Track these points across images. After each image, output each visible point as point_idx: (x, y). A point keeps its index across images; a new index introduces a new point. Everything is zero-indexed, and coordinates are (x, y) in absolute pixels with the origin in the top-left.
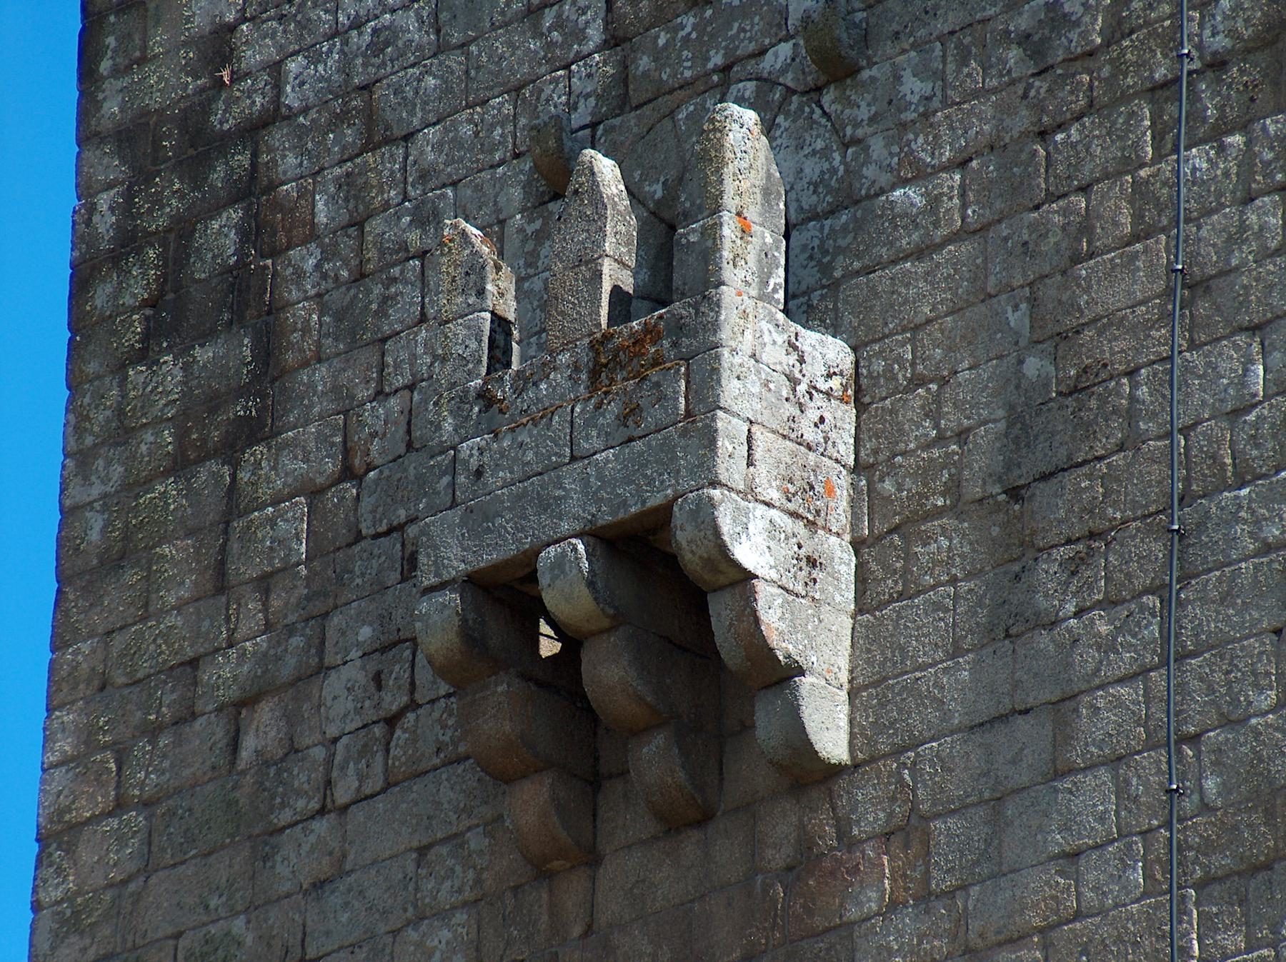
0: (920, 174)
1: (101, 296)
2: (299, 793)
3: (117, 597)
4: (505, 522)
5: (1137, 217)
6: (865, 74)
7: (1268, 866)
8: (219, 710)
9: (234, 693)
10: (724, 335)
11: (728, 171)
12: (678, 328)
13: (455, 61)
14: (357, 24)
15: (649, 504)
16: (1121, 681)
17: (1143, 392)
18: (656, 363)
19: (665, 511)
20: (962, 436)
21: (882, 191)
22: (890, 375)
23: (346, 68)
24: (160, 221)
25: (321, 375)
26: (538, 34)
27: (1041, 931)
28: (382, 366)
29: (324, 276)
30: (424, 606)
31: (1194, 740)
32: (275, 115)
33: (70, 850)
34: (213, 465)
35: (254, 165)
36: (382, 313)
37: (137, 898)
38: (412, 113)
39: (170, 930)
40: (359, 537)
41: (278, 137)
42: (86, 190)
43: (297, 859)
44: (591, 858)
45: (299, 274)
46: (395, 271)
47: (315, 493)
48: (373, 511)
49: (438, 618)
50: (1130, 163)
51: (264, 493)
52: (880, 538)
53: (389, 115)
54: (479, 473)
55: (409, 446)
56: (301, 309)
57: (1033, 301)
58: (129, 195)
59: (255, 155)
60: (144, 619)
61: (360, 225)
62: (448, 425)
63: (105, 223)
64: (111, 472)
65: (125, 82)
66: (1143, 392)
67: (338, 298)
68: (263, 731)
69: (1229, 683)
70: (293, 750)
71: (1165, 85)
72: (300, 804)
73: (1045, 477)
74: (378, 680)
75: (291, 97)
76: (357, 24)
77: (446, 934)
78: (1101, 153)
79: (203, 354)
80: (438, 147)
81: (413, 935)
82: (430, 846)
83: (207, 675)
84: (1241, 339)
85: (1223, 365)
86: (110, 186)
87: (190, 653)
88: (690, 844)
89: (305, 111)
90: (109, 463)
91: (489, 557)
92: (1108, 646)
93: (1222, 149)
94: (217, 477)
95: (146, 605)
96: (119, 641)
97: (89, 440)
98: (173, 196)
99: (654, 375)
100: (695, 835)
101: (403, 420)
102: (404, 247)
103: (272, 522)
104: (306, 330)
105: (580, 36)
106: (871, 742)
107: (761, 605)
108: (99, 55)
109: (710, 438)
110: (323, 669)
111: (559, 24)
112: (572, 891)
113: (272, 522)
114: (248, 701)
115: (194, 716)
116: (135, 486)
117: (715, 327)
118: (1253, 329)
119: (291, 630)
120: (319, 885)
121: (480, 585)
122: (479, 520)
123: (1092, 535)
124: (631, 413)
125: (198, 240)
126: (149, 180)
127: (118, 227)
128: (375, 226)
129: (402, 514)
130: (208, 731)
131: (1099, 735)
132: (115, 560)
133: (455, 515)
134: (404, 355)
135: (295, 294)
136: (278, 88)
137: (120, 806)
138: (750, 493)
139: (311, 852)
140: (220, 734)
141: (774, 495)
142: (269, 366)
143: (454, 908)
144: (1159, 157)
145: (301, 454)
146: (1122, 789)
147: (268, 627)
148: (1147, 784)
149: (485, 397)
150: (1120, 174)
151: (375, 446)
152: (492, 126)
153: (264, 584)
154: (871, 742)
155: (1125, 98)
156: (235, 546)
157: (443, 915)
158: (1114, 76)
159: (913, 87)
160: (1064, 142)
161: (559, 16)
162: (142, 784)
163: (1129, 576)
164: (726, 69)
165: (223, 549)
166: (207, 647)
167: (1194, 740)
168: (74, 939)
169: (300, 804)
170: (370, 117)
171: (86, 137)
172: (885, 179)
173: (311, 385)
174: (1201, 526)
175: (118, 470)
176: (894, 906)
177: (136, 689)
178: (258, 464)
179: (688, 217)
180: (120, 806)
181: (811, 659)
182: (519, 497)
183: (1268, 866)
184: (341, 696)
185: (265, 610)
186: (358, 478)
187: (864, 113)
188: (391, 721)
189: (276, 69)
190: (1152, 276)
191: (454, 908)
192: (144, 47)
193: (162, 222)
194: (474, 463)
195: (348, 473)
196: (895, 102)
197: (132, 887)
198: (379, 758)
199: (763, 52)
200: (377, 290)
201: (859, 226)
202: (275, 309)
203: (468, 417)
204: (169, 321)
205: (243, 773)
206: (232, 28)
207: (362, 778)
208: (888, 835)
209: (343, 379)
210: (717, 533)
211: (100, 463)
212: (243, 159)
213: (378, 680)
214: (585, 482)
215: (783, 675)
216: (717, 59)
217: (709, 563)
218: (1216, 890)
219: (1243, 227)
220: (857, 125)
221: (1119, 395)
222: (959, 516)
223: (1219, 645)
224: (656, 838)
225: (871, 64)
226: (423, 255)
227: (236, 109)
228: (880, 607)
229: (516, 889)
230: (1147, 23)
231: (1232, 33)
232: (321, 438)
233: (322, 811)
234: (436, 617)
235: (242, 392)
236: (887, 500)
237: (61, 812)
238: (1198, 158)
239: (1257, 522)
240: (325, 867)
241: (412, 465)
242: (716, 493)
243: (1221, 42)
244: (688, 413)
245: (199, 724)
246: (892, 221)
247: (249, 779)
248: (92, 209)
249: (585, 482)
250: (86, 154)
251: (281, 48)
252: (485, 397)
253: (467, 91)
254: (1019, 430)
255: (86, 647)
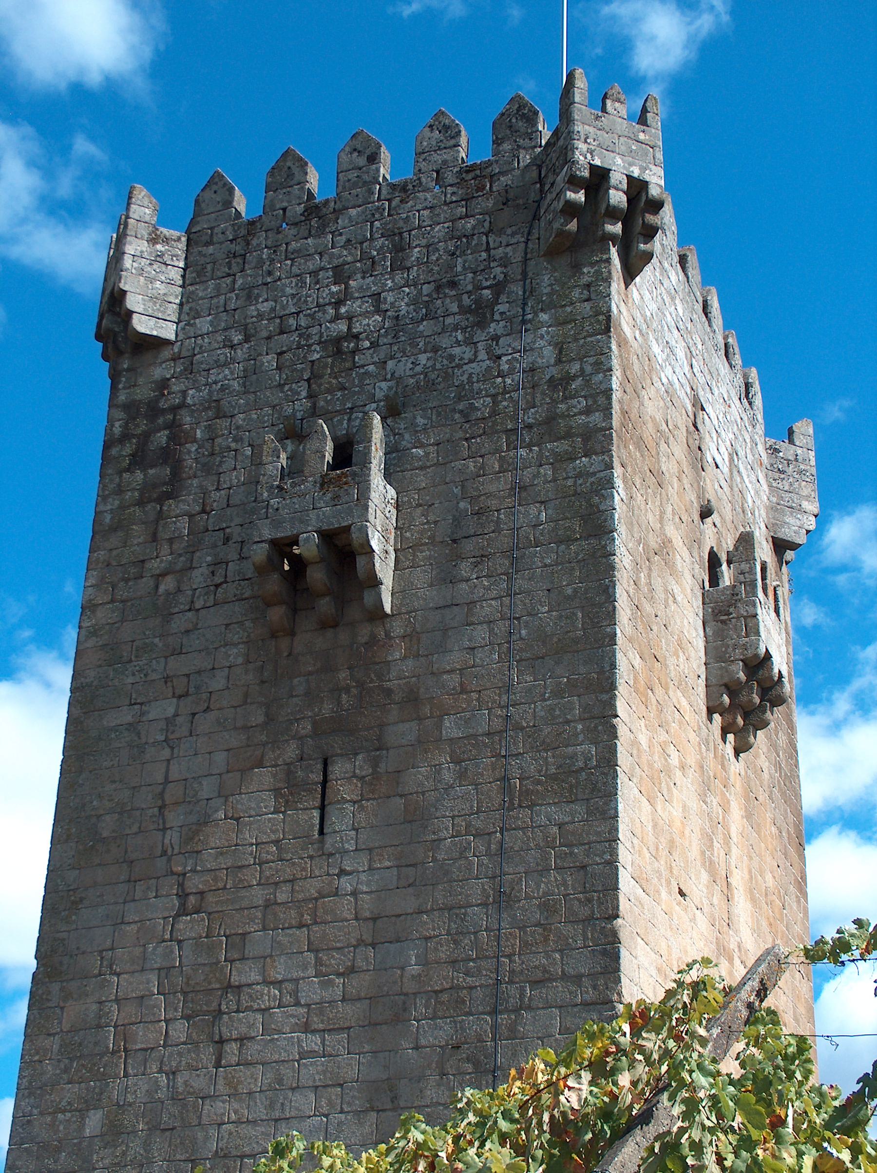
0: (422, 446)
1: (114, 451)
2: (181, 604)
3: (114, 540)
4: (287, 525)
5: (501, 466)
6: (403, 415)
7: (543, 658)
8: (152, 576)
9: (158, 572)
10: (371, 478)
11: (373, 431)
12: (354, 474)
13: (252, 397)
14: (215, 383)
15: (343, 525)
16: (492, 599)
17: (502, 516)
18: (346, 483)
19: (349, 527)
20: (436, 522)
21: (408, 449)
22: (409, 502)
23: (210, 393)
24: (139, 431)
25: (195, 482)
26: (282, 392)
27: (460, 670)
28: (219, 481)
29: (199, 453)
30: (255, 547)
31: (518, 619)
32: (183, 405)
33: (93, 612)
34: (153, 504)
35: (174, 418)
36: (220, 465)
37: (118, 628)
38: (234, 409)
39: (130, 639)
40: (207, 530)
41: (183, 412)
42: (110, 421)
43: (179, 623)
44: (293, 634)
45: (189, 452)
46: (226, 454)
47: (191, 516)
48: (214, 523)
49: (260, 552)
50: (499, 451)
51: (173, 514)
52: (404, 549)
53: (225, 409)
54: (277, 509)
55: (228, 506)
56: (189, 462)
57: (463, 487)
58: (127, 424)
59: (175, 416)
60: (124, 547)
61: (213, 440)
62: (266, 494)
63: (117, 429)
64: (114, 503)
65: (128, 391)
66: (502, 516)
67: (203, 460)
68: (168, 584)
69: (531, 604)
70: (179, 590)
71: (511, 430)
72: (182, 607)
73: (466, 537)
74: (213, 573)
75: (189, 401)
76: (215, 383)
77: (235, 651)
78: (487, 446)
79: (151, 472)
80: (244, 420)
81: (223, 650)
82: (230, 624)
83: (148, 565)
84: (537, 505)
85: (531, 512)
86: (120, 420)
87: (142, 558)
88: (330, 633)
89: (194, 405)
90: (114, 500)
91: (279, 535)
92: (488, 589)
93: (531, 450)
94: (155, 508)
95: (126, 543)
96: (115, 553)
97: (107, 492)
98: (142, 425)
99: (346, 487)
100: (332, 630)
101: (226, 498)
102: (230, 447)
103: (175, 523)
104: (191, 468)
105: (299, 394)
106: (399, 609)
107: (375, 561)
108: (119, 382)
109: (366, 508)
110: (191, 568)
111: (290, 389)
112: (284, 643)
113: (175, 523)
114: (163, 575)
115: (142, 577)
116: (122, 507)
117: (369, 475)
118: (542, 502)
119: (180, 555)
120: (187, 632)
121: (274, 543)
122: (277, 524)
123: (482, 556)
124: (336, 497)
125: (152, 438)
126: (134, 419)
127: (122, 432)
128: (219, 440)
129: (224, 525)
130: (147, 583)
131: (484, 614)
132: (114, 529)
133: (268, 521)
134: (227, 479)
135: (187, 457)
136: (185, 398)
137: (112, 601)
138: (374, 526)
139: (185, 621)
140: (152, 583)
141: (380, 529)
142: (176, 476)
143: (239, 643)
144: (508, 450)
145: (188, 503)
146: (491, 631)
147: (171, 554)
148: (500, 631)
149: (280, 488)
150: (494, 454)
151: (215, 504)
152: (264, 416)
153: (171, 541)
154: (399, 609)
155: (497, 432)
156: (161, 529)
157: (235, 645)
158: (493, 425)
159: (420, 421)
160: (475, 442)
161: (291, 387)
162: (121, 595)
163: (496, 569)
164: (352, 408)
165: (156, 529)
166: (148, 557)
167: (518, 619)
168: (94, 638)
169: (182, 607)
170: (219, 409)
171: (111, 405)
172: (409, 446)
173: (192, 484)
174: (522, 557)
175: (117, 502)
176: (405, 657)
177: (120, 568)
178: (170, 505)
179: (359, 443)
180: (112, 601)
181: (384, 581)
182: (292, 518)
183: (543, 658)
184: (199, 577)
185: (171, 548)
186: (208, 513)
187: (402, 426)
188: (217, 586)
189: (184, 393)
190: (505, 483)
191: (239, 643)
192: (135, 382)
193: (139, 432)
194: (276, 506)
195: (204, 511)
196: (414, 424)
197: (116, 625)
198: (212, 596)
199: (365, 405)
200: (218, 459)
201: (399, 459)
202: (180, 461)
203: (273, 493)
204: (138, 460)
205: (160, 596)
206: (169, 379)
207: (205, 601)
208: (404, 637)
209: (204, 483)
210: (367, 535)
211: (110, 500)
212: (171, 417)
213: (213, 573)
214: (318, 516)
215: (376, 583)
216: (349, 405)
217: (362, 546)
218: (524, 663)
219: (539, 472)
220: (399, 429)
221: (493, 516)
222: (434, 546)
223: (528, 592)
224: (316, 630)
225: (405, 413)
226: (236, 451)
227: (169, 402)
228: (404, 569)
229: (262, 640)
230: (505, 412)
231: (535, 418)
232: (194, 500)
233: (190, 610)
234: (259, 551)
235: (165, 484)
236: (408, 538)
237: (90, 600)
238: (522, 452)
239: (543, 558)
240: (191, 626)
241: (229, 511)
242: (368, 524)
243: (531, 421)
244: (358, 499)
245: (144, 580)
246: (412, 458)
247: (162, 598)
248: (113, 426)
249: (318, 516)
250: (112, 411)
251: (186, 387)
252: (280, 488)
253: (255, 405)
254: (457, 522)
255: (102, 553)
